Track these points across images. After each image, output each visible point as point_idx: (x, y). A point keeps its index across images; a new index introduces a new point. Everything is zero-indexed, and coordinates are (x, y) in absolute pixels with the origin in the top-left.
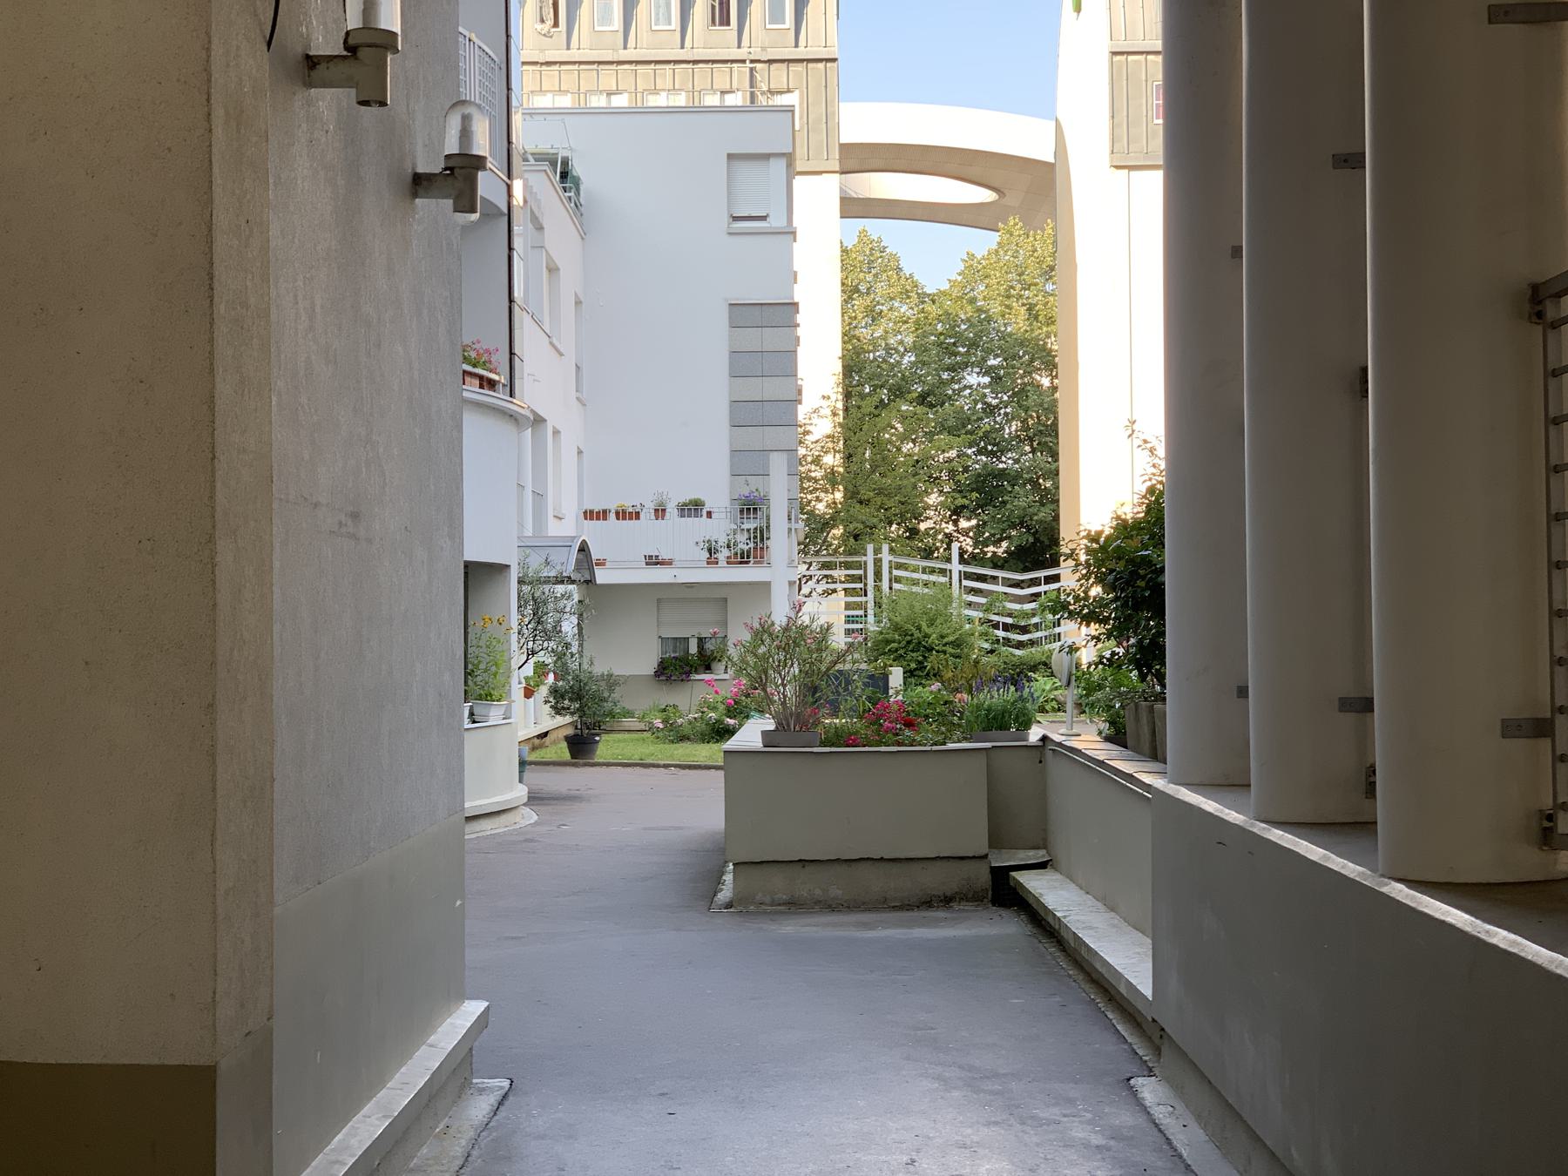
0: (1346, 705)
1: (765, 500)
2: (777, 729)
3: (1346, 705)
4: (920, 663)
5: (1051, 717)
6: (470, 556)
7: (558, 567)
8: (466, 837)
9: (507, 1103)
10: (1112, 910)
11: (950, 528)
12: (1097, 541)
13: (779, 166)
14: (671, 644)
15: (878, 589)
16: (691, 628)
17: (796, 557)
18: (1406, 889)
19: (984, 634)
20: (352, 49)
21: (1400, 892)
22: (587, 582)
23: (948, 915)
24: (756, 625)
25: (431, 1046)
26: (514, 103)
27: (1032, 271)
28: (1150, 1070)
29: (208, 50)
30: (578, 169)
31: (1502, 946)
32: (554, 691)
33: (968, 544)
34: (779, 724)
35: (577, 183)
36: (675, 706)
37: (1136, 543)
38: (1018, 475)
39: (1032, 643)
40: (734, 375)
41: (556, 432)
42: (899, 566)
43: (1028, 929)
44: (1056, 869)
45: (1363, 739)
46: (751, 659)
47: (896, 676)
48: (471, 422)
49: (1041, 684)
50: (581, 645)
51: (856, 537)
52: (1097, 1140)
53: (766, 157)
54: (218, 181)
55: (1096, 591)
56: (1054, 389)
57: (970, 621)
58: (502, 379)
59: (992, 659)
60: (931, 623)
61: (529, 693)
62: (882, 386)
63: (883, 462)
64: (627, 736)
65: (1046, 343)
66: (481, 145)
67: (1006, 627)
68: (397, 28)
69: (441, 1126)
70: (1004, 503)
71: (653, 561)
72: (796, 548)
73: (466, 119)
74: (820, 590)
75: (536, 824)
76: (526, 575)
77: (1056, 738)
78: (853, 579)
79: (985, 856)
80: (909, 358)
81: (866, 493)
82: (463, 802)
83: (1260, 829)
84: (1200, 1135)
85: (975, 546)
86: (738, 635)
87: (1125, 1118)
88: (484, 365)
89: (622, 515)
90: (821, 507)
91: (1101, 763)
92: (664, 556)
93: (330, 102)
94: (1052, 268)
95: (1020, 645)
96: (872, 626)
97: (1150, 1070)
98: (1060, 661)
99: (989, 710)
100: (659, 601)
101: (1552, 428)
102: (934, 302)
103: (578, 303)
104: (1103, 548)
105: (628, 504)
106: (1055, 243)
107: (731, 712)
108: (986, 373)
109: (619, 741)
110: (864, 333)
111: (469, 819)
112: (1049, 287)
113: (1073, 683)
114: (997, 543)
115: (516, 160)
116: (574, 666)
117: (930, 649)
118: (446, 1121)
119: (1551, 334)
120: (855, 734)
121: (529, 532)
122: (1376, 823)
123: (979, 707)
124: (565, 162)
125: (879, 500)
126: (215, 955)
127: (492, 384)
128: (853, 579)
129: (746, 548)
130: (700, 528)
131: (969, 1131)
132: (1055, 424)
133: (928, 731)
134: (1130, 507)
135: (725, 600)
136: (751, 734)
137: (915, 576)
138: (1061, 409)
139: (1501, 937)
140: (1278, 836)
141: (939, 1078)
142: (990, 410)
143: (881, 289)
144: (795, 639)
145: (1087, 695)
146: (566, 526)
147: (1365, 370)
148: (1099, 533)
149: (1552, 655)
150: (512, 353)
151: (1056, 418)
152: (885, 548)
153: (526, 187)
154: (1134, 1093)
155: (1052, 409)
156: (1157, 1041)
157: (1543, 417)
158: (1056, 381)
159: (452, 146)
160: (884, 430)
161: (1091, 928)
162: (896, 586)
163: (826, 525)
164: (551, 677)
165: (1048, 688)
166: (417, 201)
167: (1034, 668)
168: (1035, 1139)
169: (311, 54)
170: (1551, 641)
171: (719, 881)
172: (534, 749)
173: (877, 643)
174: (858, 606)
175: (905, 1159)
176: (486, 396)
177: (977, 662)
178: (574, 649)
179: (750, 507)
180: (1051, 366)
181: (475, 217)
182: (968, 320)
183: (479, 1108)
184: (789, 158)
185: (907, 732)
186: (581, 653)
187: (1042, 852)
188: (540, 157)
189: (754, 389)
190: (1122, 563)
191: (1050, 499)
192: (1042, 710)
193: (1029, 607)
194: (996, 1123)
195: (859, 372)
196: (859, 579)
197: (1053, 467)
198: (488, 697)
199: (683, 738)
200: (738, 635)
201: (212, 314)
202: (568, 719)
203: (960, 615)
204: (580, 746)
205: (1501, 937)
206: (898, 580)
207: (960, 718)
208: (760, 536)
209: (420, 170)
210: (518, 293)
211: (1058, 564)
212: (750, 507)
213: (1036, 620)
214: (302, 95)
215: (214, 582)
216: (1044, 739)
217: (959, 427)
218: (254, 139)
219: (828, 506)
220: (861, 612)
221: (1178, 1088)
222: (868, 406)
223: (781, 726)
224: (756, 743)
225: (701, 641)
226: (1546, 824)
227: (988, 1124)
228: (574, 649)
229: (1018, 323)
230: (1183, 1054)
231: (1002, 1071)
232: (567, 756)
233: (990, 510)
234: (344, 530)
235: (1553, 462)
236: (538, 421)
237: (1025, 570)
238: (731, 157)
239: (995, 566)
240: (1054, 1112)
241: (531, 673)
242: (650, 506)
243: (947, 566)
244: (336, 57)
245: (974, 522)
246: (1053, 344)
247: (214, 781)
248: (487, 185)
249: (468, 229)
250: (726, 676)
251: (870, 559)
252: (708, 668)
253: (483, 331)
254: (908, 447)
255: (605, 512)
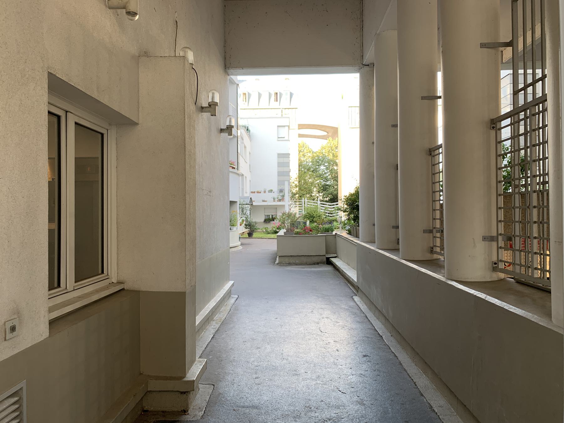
0: (393, 227)
1: (284, 190)
2: (286, 231)
3: (393, 227)
4: (312, 220)
5: (337, 230)
6: (231, 200)
7: (246, 202)
8: (230, 251)
9: (238, 300)
10: (349, 265)
11: (318, 195)
12: (346, 197)
13: (287, 128)
14: (267, 216)
15: (305, 206)
16: (270, 213)
17: (289, 200)
18: (405, 261)
19: (324, 214)
20: (210, 105)
21: (404, 262)
22: (251, 205)
23: (318, 266)
24: (283, 212)
25: (224, 289)
26: (238, 116)
27: (334, 147)
28: (356, 295)
29: (184, 105)
30: (250, 128)
31: (424, 272)
32: (246, 225)
33: (321, 198)
34: (287, 230)
35: (249, 131)
36: (267, 228)
37: (353, 197)
38: (331, 185)
39: (333, 216)
40: (278, 167)
41: (246, 177)
42: (309, 202)
43: (333, 269)
44: (338, 258)
45: (397, 234)
46: (282, 219)
47: (308, 222)
48: (231, 174)
49: (335, 223)
50: (250, 216)
51: (300, 197)
52: (346, 308)
53: (284, 126)
54: (186, 129)
55: (346, 206)
56: (337, 169)
57: (322, 212)
58: (236, 167)
59: (326, 219)
60: (314, 212)
61: (241, 225)
62: (305, 169)
63: (306, 183)
64: (259, 233)
65: (336, 161)
66: (233, 123)
67: (328, 213)
68: (218, 101)
69: (226, 304)
70: (328, 190)
71: (264, 201)
72: (290, 199)
73: (230, 119)
74: (294, 206)
75: (242, 249)
76: (240, 203)
77: (338, 233)
78: (300, 204)
79: (325, 255)
80: (311, 164)
81: (302, 189)
82: (229, 244)
83: (377, 250)
84: (366, 307)
85: (322, 198)
86: (279, 214)
87: (352, 304)
88: (233, 165)
89: (258, 192)
90: (294, 191)
91: (347, 238)
92: (265, 200)
93: (206, 115)
94: (337, 147)
95: (331, 217)
96: (303, 213)
97: (356, 295)
98: (339, 219)
99: (326, 228)
100: (264, 208)
101: (433, 176)
102: (315, 153)
103: (250, 153)
104: (347, 198)
105: (259, 190)
106: (338, 142)
107: (278, 229)
108: (325, 166)
109: (257, 234)
110: (302, 159)
111: (230, 248)
112: (337, 150)
113: (341, 224)
114: (326, 198)
115: (239, 127)
116: (249, 220)
117: (314, 217)
118: (226, 303)
119: (433, 158)
120: (301, 232)
121: (241, 195)
122: (399, 249)
123: (324, 228)
124: (247, 127)
125: (305, 190)
126: (185, 272)
127: (234, 168)
128: (300, 204)
129: (280, 199)
130: (272, 195)
131: (323, 306)
132: (337, 176)
133: (314, 233)
134: (353, 191)
135: (277, 208)
136: (282, 232)
137: (311, 204)
138: (339, 173)
139: (423, 270)
140: (381, 251)
141: (317, 296)
142: (325, 173)
143: (305, 151)
144: (289, 215)
145: (344, 226)
146: (248, 194)
147: (397, 165)
148: (347, 196)
149: (432, 182)
150: (238, 162)
151: (338, 175)
152: (306, 198)
153: (241, 133)
154: (353, 299)
155: (337, 173)
156: (357, 289)
157: (431, 164)
158: (338, 168)
159: (228, 124)
160: (306, 177)
161: (345, 269)
162: (308, 206)
163: (295, 194)
164: (245, 222)
165: (336, 224)
166: (221, 134)
167: (333, 221)
168: (335, 307)
169: (202, 106)
170: (433, 216)
171: (276, 259)
172: (242, 235)
173: (304, 216)
174: (301, 209)
175: (311, 311)
176: (233, 170)
177: (323, 219)
178: (249, 217)
179: (281, 191)
180: (337, 165)
181: (232, 137)
182: (322, 156)
183: (232, 301)
184: (289, 126)
185: (310, 232)
186: (250, 218)
187: (336, 255)
188: (243, 126)
189: (282, 169)
190: (351, 201)
191: (337, 190)
192: (335, 229)
193: (333, 209)
194: (328, 304)
195: (301, 166)
196: (301, 204)
197: (337, 184)
198: (233, 225)
199: (269, 233)
200: (279, 214)
201: (185, 154)
202: (248, 230)
203: (320, 211)
204: (250, 235)
205: (423, 270)
206: (308, 204)
207: (320, 230)
208: (283, 196)
209: (222, 128)
210: (239, 151)
211: (337, 201)
212: (281, 191)
213: (334, 212)
214: (201, 114)
215: (185, 203)
216: (336, 234)
217: (320, 176)
218: (193, 121)
219: (296, 191)
220: (301, 210)
221: (361, 298)
222: (303, 173)
223: (287, 231)
224: (283, 234)
225: (272, 215)
226: (432, 249)
227: (326, 304)
228: (249, 217)
229: (331, 157)
230: (363, 292)
231: (329, 295)
232: (248, 236)
233: (325, 192)
234: (208, 194)
235: (433, 182)
236: (243, 175)
237: (332, 203)
238: (278, 126)
239: (326, 202)
240: (338, 302)
241: (241, 221)
242: (263, 191)
243: (317, 202)
244: (206, 107)
245: (322, 194)
246: (337, 161)
247: (186, 239)
248: (234, 131)
249: (230, 139)
250: (277, 222)
251: (303, 201)
252: (273, 220)
253: (233, 158)
254: (310, 180)
255: (255, 192)
